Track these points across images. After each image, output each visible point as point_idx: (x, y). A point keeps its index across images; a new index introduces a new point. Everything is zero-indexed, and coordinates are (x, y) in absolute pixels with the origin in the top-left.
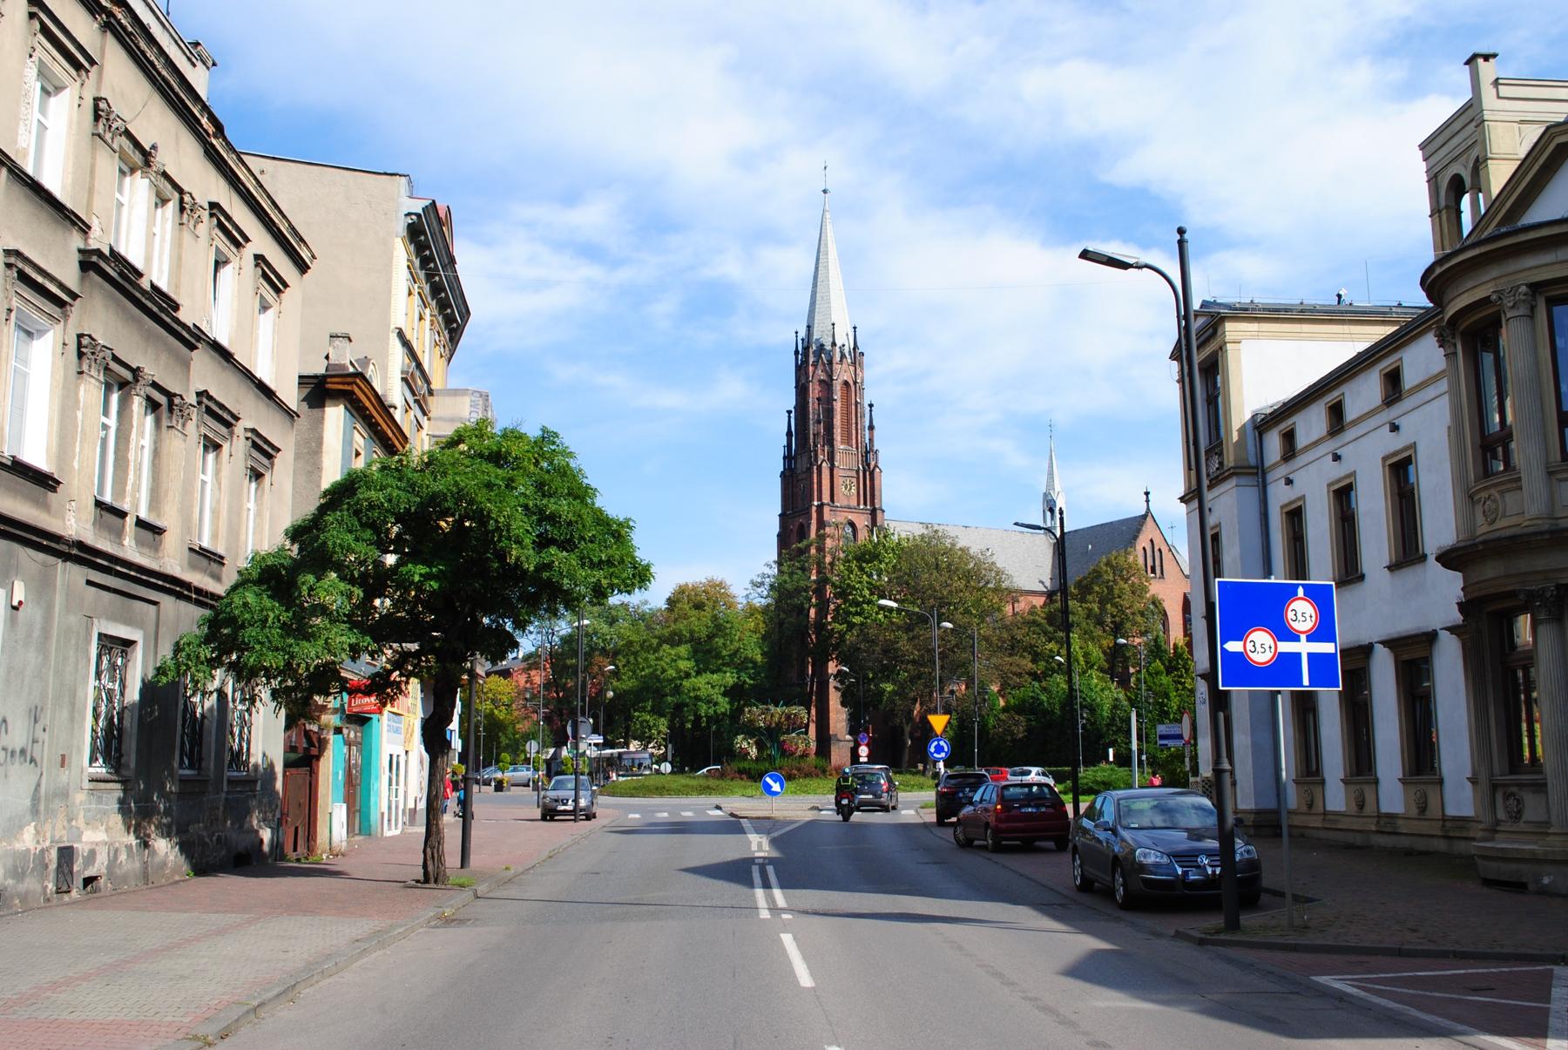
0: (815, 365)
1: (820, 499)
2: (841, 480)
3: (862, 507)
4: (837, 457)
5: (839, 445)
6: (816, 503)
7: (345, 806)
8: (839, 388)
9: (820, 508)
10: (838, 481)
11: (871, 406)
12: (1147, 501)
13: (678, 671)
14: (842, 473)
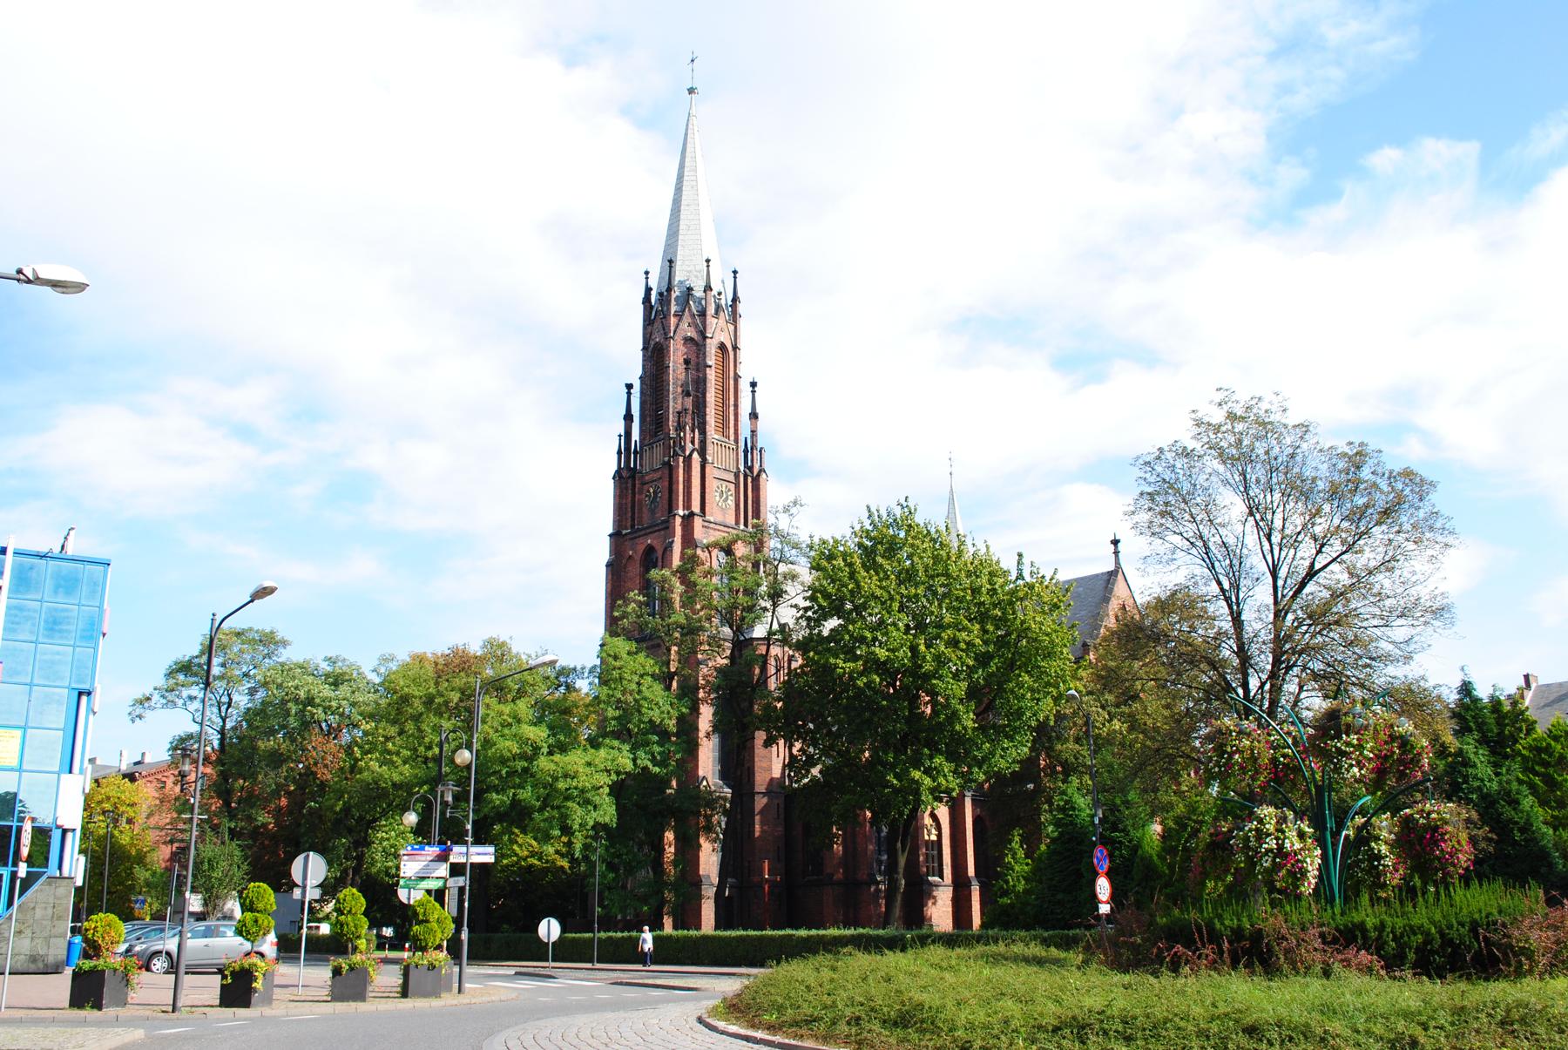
0: (679, 316)
1: (688, 505)
2: (716, 483)
3: (742, 527)
4: (710, 449)
5: (712, 434)
6: (681, 512)
7: (701, 873)
8: (713, 351)
9: (688, 519)
10: (712, 484)
11: (753, 385)
12: (1116, 553)
13: (523, 741)
14: (718, 474)
